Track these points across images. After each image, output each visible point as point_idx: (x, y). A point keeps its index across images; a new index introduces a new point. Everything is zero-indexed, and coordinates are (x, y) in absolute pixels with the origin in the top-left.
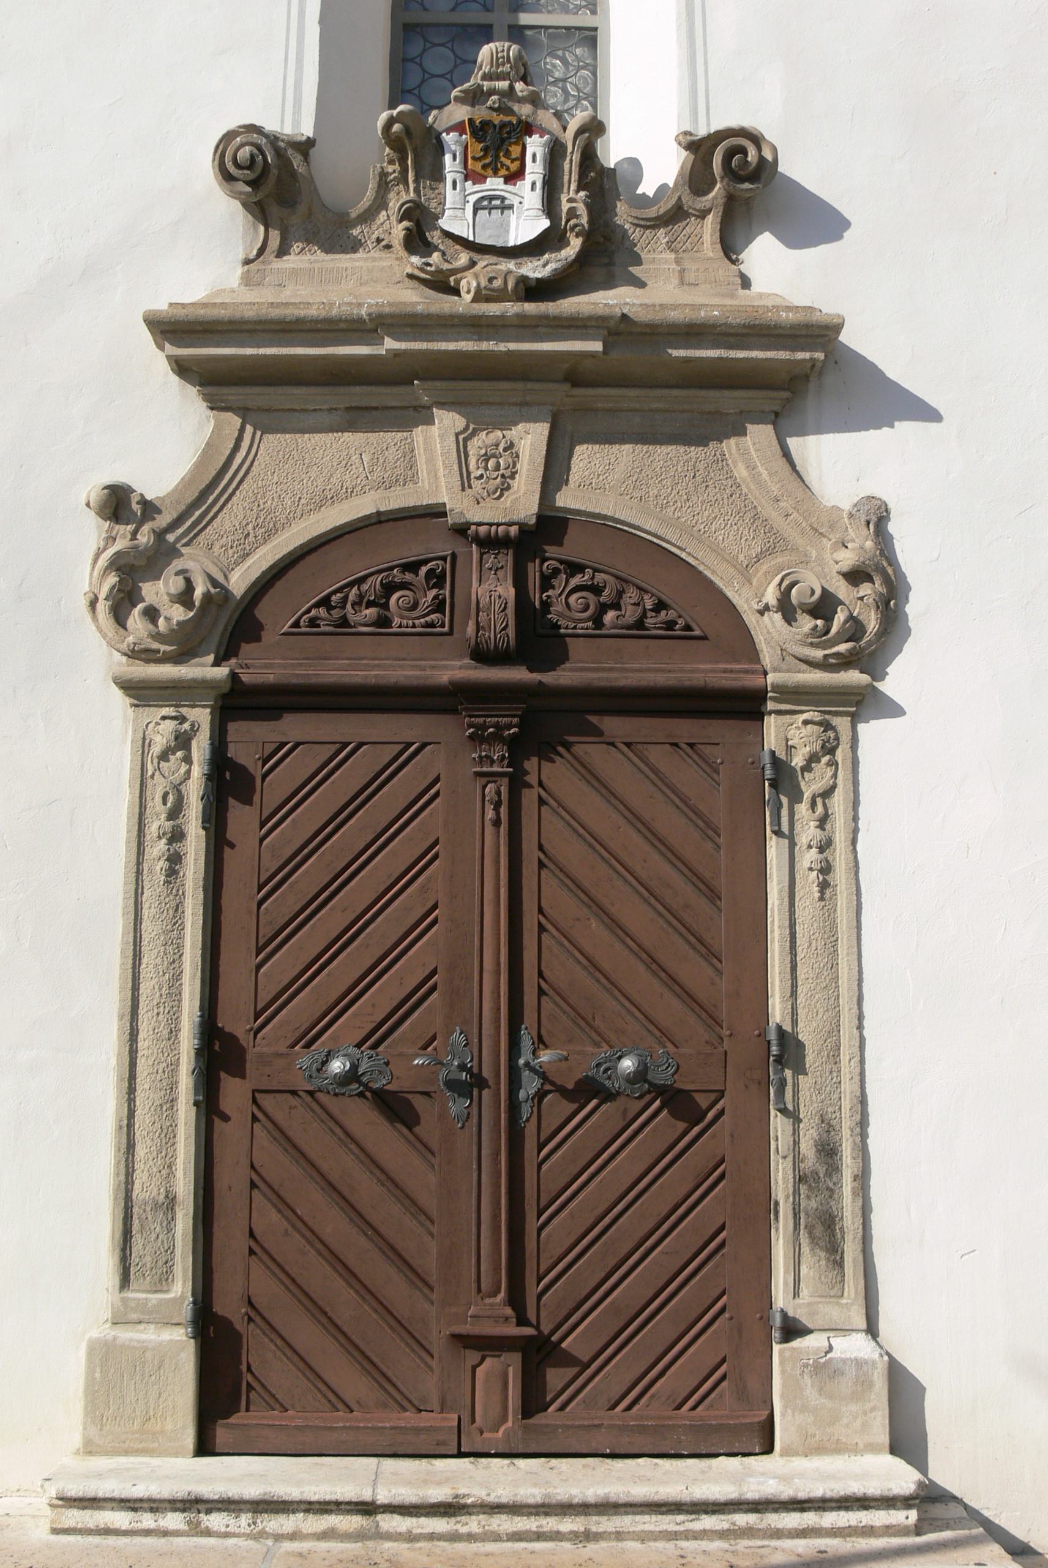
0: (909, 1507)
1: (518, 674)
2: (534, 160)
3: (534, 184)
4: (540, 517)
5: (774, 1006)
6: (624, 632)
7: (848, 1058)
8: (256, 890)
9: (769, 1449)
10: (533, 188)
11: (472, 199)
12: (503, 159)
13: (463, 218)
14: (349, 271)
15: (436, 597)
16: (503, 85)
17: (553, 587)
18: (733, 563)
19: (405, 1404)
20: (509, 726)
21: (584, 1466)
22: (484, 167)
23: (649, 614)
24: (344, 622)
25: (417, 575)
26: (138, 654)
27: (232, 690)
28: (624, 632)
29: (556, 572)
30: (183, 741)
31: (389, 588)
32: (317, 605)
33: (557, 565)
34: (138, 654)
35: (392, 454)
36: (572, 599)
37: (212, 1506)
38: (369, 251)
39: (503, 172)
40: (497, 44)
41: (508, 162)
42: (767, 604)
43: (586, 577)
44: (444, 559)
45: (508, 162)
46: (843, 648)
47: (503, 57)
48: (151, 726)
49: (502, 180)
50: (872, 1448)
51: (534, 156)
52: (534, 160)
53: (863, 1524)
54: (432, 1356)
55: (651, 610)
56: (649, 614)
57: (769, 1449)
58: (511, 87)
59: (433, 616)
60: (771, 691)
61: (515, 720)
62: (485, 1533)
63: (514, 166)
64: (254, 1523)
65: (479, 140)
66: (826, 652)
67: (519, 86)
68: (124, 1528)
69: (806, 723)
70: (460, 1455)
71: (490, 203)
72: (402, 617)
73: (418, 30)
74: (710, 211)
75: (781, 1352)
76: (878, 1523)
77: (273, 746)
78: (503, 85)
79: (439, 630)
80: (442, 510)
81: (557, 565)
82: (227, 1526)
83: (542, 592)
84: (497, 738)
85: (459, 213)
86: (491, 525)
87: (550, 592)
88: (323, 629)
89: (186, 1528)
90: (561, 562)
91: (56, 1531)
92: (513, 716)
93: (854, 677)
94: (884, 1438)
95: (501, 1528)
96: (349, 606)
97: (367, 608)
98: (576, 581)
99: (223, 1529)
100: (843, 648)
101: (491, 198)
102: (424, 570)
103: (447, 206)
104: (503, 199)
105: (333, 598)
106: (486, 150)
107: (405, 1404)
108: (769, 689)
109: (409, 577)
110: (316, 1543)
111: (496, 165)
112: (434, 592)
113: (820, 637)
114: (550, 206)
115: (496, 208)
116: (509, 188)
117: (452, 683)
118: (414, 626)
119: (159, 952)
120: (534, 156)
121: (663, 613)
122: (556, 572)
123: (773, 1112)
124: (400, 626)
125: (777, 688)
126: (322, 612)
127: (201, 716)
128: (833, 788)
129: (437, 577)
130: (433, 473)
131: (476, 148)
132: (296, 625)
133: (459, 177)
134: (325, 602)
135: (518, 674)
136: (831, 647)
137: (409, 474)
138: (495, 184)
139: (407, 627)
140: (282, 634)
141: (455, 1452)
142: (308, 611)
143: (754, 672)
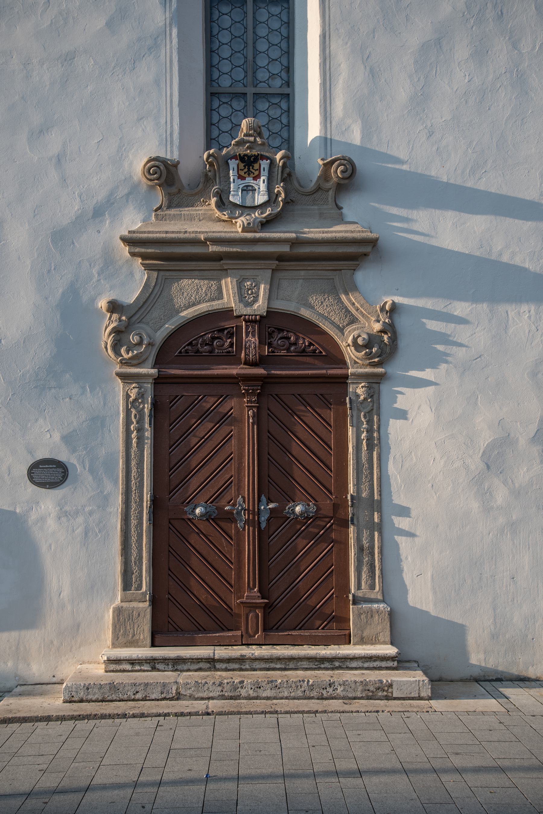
0: (394, 661)
1: (260, 371)
2: (264, 170)
3: (264, 180)
4: (267, 312)
5: (350, 487)
6: (299, 354)
7: (376, 506)
8: (168, 448)
9: (349, 643)
10: (264, 182)
11: (241, 186)
12: (251, 170)
13: (238, 195)
14: (195, 215)
15: (230, 342)
16: (252, 139)
17: (273, 338)
18: (338, 327)
19: (224, 628)
20: (258, 389)
21: (285, 647)
22: (245, 173)
23: (307, 347)
24: (198, 351)
25: (223, 334)
26: (125, 363)
27: (158, 377)
28: (299, 354)
29: (273, 331)
30: (141, 395)
31: (213, 339)
32: (188, 345)
33: (274, 329)
34: (125, 363)
35: (214, 287)
36: (279, 342)
37: (160, 661)
38: (202, 206)
39: (252, 175)
40: (249, 119)
41: (253, 171)
42: (349, 344)
43: (284, 334)
44: (233, 327)
45: (253, 171)
46: (376, 360)
47: (251, 126)
48: (129, 390)
49: (252, 178)
50: (385, 643)
51: (264, 168)
52: (264, 170)
53: (378, 666)
54: (232, 539)
55: (307, 346)
56: (307, 347)
57: (349, 643)
58: (255, 139)
59: (230, 349)
60: (350, 376)
61: (259, 387)
62: (251, 668)
63: (256, 173)
64: (174, 667)
65: (243, 162)
66: (371, 361)
67: (258, 139)
68: (130, 669)
69: (362, 387)
70: (243, 645)
71: (247, 188)
72: (218, 350)
73: (217, 95)
74: (331, 189)
75: (353, 608)
76: (383, 666)
77: (173, 397)
78: (252, 139)
79: (232, 354)
80: (232, 309)
81: (274, 329)
82: (165, 668)
83: (269, 339)
84: (253, 394)
85: (235, 193)
86: (250, 315)
87: (272, 340)
88: (190, 354)
89: (151, 669)
90: (275, 328)
91: (106, 671)
92: (259, 386)
93: (380, 370)
94: (388, 639)
95: (256, 667)
96: (199, 345)
97: (205, 346)
98: (280, 336)
99: (163, 669)
100: (376, 360)
101: (247, 186)
102: (226, 332)
103: (231, 190)
104: (252, 186)
105: (193, 342)
106: (245, 166)
107: (224, 628)
108: (349, 375)
109: (220, 335)
110: (195, 673)
111: (249, 173)
112: (229, 341)
113: (369, 356)
114: (270, 189)
115: (250, 190)
116: (255, 182)
117: (237, 374)
118: (223, 352)
119: (135, 471)
120: (264, 168)
121: (312, 347)
122: (273, 331)
123: (350, 524)
124: (218, 353)
125: (352, 374)
126: (190, 347)
127: (149, 386)
128: (372, 410)
129: (231, 334)
130: (228, 294)
131: (242, 166)
132: (180, 352)
133: (236, 178)
134: (190, 344)
135: (260, 371)
136: (372, 359)
137: (220, 296)
138: (249, 180)
139: (220, 353)
140: (176, 356)
141: (241, 644)
142: (185, 347)
143: (345, 368)
